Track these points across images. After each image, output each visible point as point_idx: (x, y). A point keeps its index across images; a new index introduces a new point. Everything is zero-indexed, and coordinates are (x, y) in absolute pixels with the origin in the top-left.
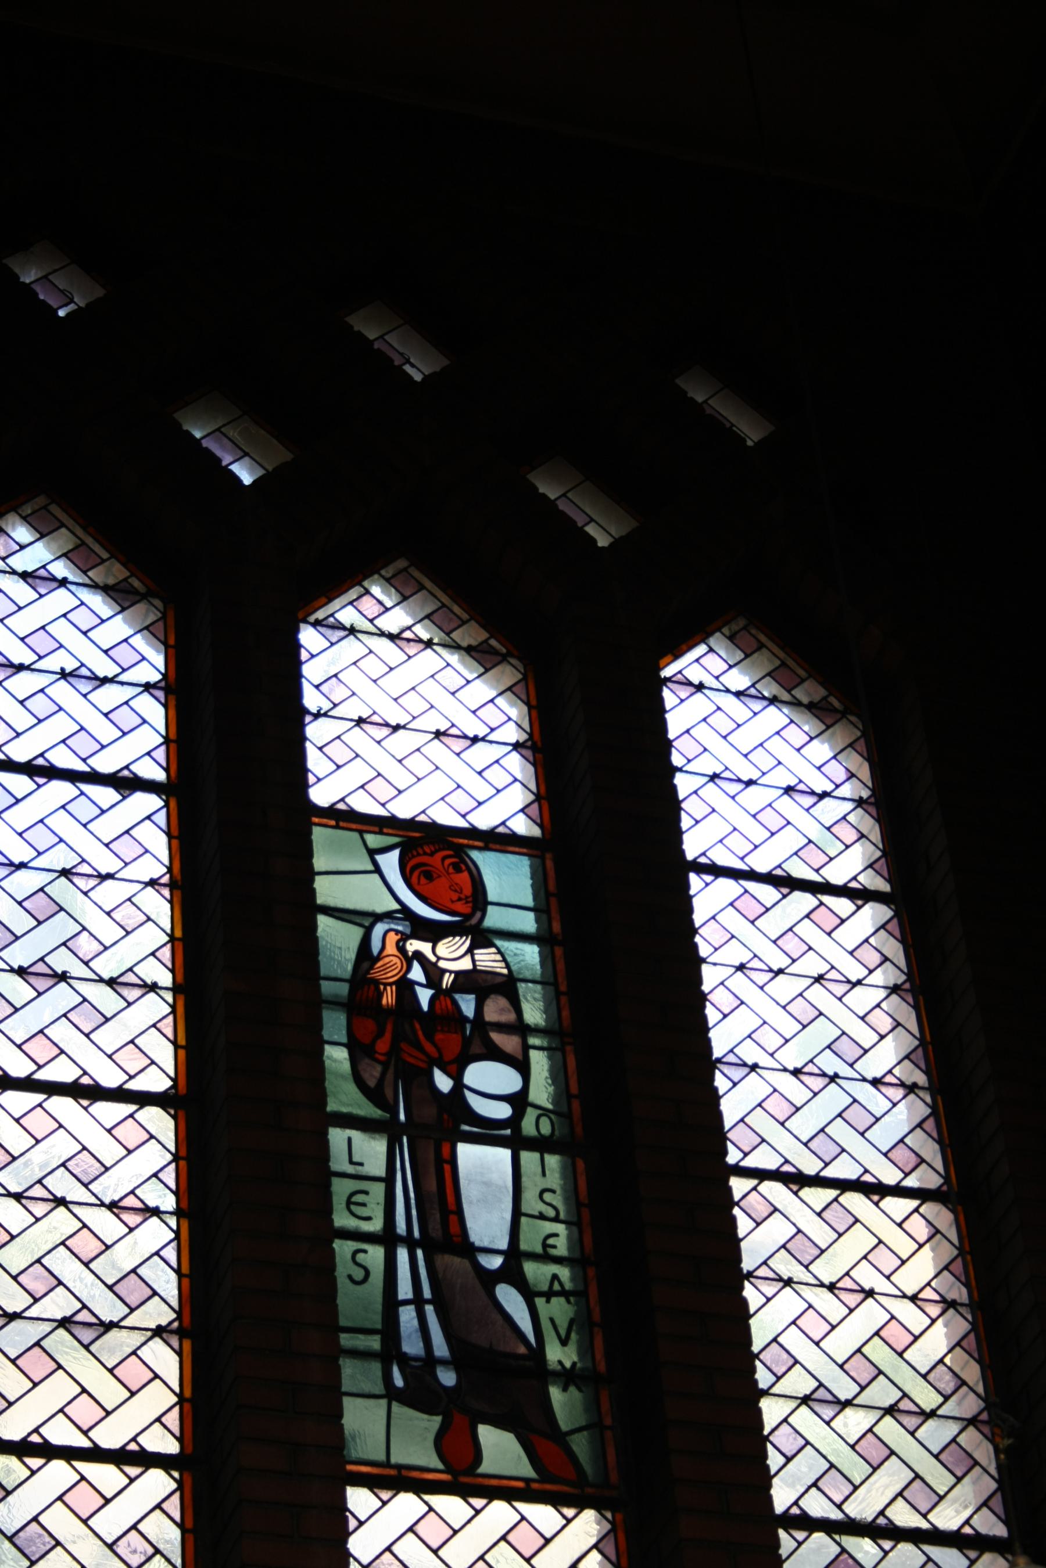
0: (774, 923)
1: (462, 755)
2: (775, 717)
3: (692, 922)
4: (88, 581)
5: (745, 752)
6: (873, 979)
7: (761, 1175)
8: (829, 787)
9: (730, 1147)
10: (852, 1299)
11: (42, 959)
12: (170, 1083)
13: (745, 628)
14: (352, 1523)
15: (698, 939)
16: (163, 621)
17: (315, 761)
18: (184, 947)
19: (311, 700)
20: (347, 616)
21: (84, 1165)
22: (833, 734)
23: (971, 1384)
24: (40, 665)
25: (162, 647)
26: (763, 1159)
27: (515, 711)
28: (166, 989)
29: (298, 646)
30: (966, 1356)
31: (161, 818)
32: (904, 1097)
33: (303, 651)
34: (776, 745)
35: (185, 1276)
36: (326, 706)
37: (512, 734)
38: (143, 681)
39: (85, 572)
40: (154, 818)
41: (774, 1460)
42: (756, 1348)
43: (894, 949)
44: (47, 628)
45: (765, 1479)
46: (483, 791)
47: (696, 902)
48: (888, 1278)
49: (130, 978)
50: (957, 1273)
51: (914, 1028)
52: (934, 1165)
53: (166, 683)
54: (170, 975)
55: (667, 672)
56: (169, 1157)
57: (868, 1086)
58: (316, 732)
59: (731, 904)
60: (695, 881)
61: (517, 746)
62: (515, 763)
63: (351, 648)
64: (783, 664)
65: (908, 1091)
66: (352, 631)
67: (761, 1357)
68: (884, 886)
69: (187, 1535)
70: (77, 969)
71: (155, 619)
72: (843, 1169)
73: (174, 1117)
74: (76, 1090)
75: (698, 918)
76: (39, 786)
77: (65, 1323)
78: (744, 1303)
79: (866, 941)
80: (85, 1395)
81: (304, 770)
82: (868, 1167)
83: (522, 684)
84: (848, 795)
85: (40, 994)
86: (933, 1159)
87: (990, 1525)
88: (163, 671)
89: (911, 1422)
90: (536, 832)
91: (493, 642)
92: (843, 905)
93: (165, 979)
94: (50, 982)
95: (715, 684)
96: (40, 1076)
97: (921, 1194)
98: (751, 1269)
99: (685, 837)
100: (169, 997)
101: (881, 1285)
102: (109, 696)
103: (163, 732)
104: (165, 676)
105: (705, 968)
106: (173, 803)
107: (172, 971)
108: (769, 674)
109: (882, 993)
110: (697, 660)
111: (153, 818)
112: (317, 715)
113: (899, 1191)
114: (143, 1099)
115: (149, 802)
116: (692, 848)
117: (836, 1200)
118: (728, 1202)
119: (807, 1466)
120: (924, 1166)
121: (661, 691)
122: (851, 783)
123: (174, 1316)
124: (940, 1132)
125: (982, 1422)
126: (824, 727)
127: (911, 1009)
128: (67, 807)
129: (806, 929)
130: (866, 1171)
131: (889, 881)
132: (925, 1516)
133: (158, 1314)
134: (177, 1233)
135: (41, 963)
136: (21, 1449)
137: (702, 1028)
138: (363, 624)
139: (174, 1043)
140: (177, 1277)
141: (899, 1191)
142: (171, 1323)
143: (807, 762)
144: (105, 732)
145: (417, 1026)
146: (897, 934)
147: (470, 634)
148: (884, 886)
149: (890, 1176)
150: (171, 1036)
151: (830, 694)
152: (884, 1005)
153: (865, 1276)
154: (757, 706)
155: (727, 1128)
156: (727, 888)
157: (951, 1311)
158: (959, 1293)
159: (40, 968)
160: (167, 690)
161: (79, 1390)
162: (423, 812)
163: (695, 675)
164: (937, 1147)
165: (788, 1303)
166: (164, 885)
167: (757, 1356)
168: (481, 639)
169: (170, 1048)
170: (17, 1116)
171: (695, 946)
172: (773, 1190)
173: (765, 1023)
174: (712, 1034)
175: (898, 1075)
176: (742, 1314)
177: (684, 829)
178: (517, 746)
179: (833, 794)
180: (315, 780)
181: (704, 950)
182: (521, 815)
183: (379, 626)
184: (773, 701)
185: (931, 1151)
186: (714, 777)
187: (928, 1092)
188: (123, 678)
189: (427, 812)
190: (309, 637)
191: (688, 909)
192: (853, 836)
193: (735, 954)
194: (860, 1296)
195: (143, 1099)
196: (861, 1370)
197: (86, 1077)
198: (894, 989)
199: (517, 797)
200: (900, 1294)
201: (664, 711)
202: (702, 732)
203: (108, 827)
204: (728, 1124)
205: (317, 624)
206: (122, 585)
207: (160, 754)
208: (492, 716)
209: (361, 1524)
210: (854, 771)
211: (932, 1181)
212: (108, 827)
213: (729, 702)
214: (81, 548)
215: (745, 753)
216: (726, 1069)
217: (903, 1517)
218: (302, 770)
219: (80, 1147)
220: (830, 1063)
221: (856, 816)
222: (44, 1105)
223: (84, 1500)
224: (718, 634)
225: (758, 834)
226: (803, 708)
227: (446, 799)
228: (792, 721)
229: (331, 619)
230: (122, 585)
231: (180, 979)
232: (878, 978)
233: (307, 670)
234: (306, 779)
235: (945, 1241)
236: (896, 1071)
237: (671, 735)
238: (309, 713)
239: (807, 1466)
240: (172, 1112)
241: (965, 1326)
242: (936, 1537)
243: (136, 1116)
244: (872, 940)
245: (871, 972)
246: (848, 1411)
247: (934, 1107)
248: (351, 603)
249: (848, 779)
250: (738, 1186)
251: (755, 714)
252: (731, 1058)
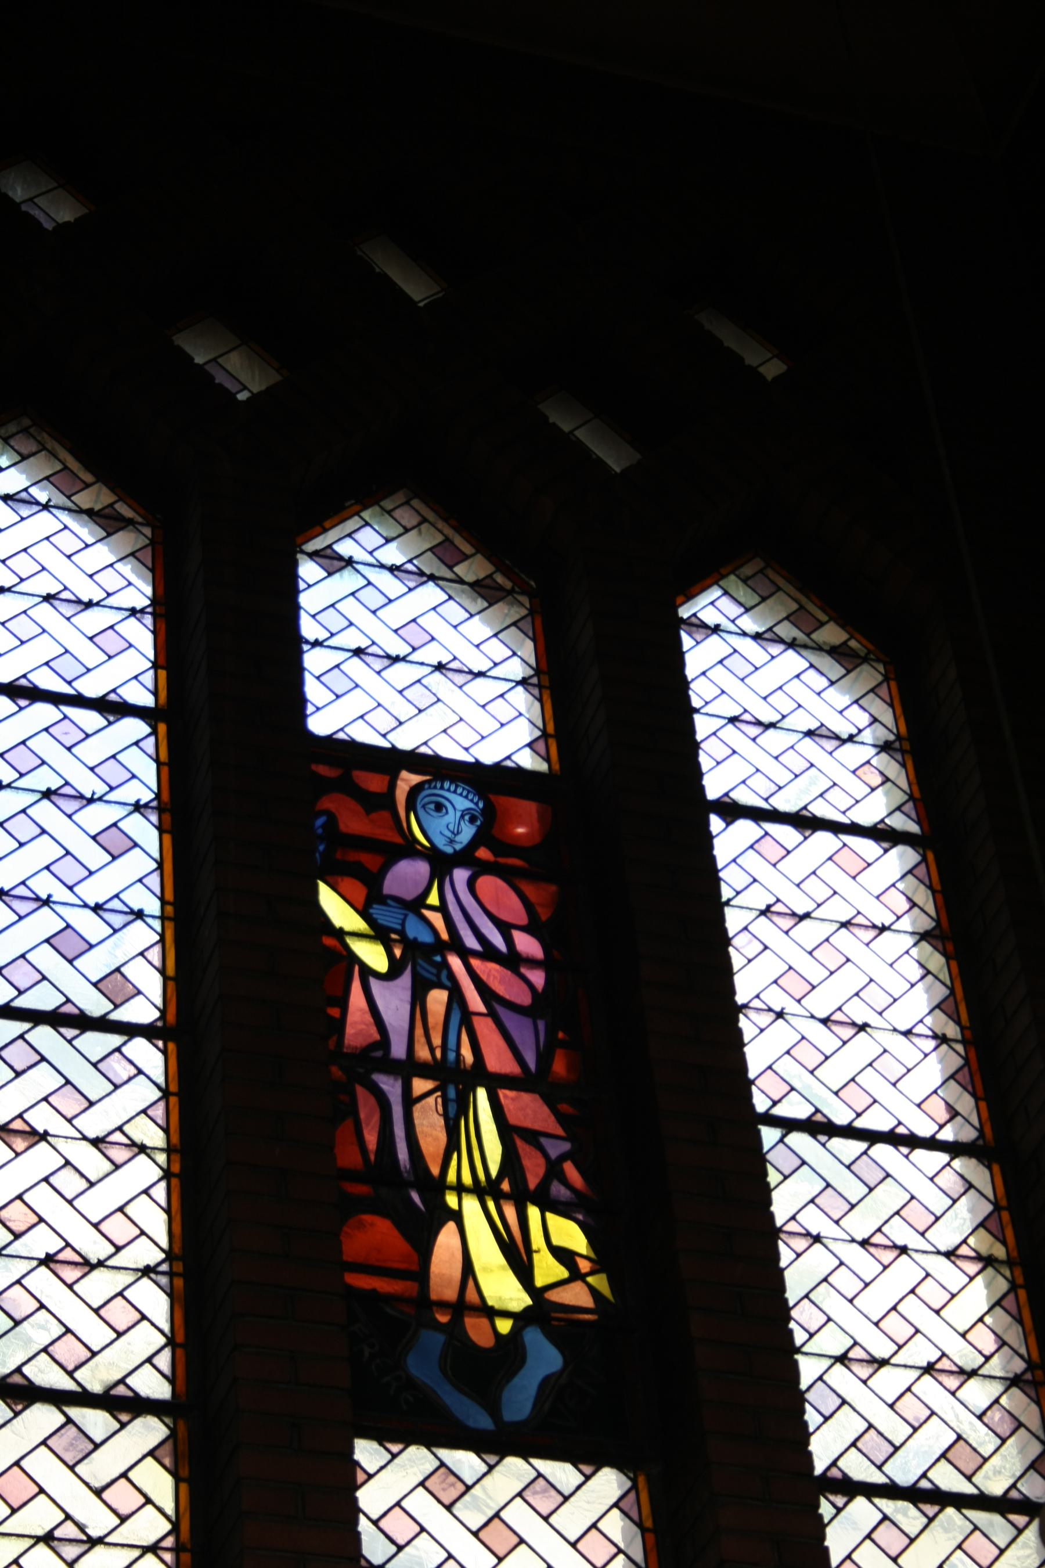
0: (797, 865)
1: (464, 688)
2: (793, 661)
3: (725, 931)
4: (69, 504)
5: (775, 755)
6: (900, 925)
7: (789, 1125)
8: (809, 906)
9: (770, 1169)
10: (887, 1256)
11: (23, 883)
12: (157, 1014)
13: (761, 571)
14: (361, 1477)
15: (691, 693)
16: (164, 1100)
17: (313, 690)
18: (170, 770)
19: (309, 629)
20: (346, 548)
21: (69, 871)
22: (855, 680)
23: (921, 904)
24: (22, 587)
25: (150, 575)
26: (794, 1109)
27: (528, 650)
28: (153, 917)
29: (294, 577)
30: (959, 1089)
31: (149, 744)
32: (935, 1049)
33: (309, 705)
34: (795, 688)
35: (164, 764)
36: (322, 635)
37: (516, 669)
38: (129, 605)
39: (69, 497)
40: (141, 744)
41: (812, 1418)
42: (752, 1075)
43: (924, 896)
44: (28, 956)
45: (804, 1435)
46: (487, 724)
47: (688, 658)
48: (923, 1234)
49: (116, 904)
50: (921, 876)
51: (903, 783)
52: (971, 1121)
53: (159, 803)
54: (161, 1134)
55: (685, 612)
56: (162, 1340)
57: (943, 1260)
58: (314, 661)
59: (775, 982)
60: (716, 823)
61: (523, 682)
62: (520, 698)
63: (346, 581)
64: (801, 607)
65: (939, 1041)
66: (716, 629)
67: (757, 1082)
68: (914, 828)
69: (173, 1157)
70: (61, 894)
71: (144, 544)
72: (876, 1121)
73: (164, 1052)
74: (55, 1019)
75: (690, 672)
76: (21, 709)
77: (48, 1261)
78: (740, 1033)
79: (893, 885)
80: (69, 1197)
81: (303, 701)
82: (921, 1238)
83: (529, 619)
84: (999, 1373)
85: (21, 918)
86: (925, 904)
87: (900, 822)
88: (156, 790)
89: (864, 1371)
90: (543, 767)
91: (853, 644)
92: (868, 848)
93: (153, 906)
94: (34, 905)
95: (732, 627)
96: (22, 1026)
97: (954, 1149)
98: (745, 1001)
99: (716, 841)
100: (157, 925)
101: (913, 1241)
102: (94, 620)
103: (152, 658)
104: (158, 796)
105: (697, 717)
106: (930, 856)
107: (166, 1130)
108: (787, 618)
109: (910, 941)
110: (712, 603)
111: (141, 744)
112: (317, 643)
113: (931, 1144)
114: (130, 1030)
115: (135, 728)
116: (714, 788)
117: (865, 1153)
118: (759, 1161)
119: (847, 1425)
120: (1022, 1430)
121: (737, 1020)
122: (991, 1317)
123: (153, 796)
124: (973, 1087)
125: (1027, 1382)
126: (844, 671)
127: (886, 706)
128: (51, 664)
129: (829, 872)
130: (907, 1157)
131: (919, 822)
132: (969, 1478)
133: (148, 1254)
134: (162, 936)
135: (22, 913)
136: (13, 690)
137: (726, 972)
138: (359, 555)
139: (157, 761)
140: (153, 636)
141: (931, 1144)
142: (159, 1264)
143: (866, 887)
144: (91, 655)
145: (410, 838)
146: (913, 815)
147: (831, 634)
148: (914, 828)
149: (924, 1129)
150: (158, 891)
151: (852, 637)
152: (988, 1320)
153: (898, 1231)
154: (775, 649)
155: (765, 1149)
156: (745, 829)
157: (944, 1047)
158: (952, 1030)
159: (22, 891)
160: (160, 810)
161: (63, 1081)
162: (425, 743)
163: (710, 617)
164: (929, 892)
165: (781, 1035)
166: (163, 1273)
167: (752, 1082)
168: (489, 572)
169: (153, 766)
170: (95, 1220)
171: (688, 698)
172: (799, 1140)
173: (803, 1038)
174: (746, 1049)
175: (972, 1245)
176: (736, 1042)
177: (714, 833)
178: (523, 682)
179: (409, 658)
180: (314, 709)
181: (696, 702)
182: (527, 750)
183: (380, 559)
184: (792, 645)
185: (966, 1104)
186: (733, 720)
187: (512, 1202)
188: (332, 642)
189: (429, 743)
190: (308, 570)
191: (780, 1286)
192: (877, 780)
193: (758, 898)
194: (894, 1253)
195: (130, 1030)
196: (909, 1407)
197: (69, 1005)
198: (923, 937)
199: (523, 732)
200: (766, 1008)
201: (700, 775)
202: (719, 674)
203: (93, 751)
204: (720, 864)
205: (313, 555)
206: (107, 511)
207: (148, 679)
208: (110, 580)
209: (370, 1476)
210: (876, 715)
211: (968, 1135)
212: (93, 751)
213: (748, 646)
214: (64, 472)
215: (775, 755)
216: (752, 1014)
217: (948, 1479)
218: (302, 701)
219: (63, 1244)
220: (858, 1013)
221: (1009, 1398)
222: (26, 1036)
223: (69, 1351)
224: (732, 577)
225: (782, 776)
226: (824, 654)
227: (438, 609)
228: (812, 666)
229: (329, 551)
230: (107, 511)
231: (175, 1139)
232: (905, 924)
233: (304, 599)
234: (296, 585)
235: (895, 788)
236: (971, 1241)
237: (699, 737)
238: (307, 642)
239: (847, 1425)
240: (160, 1044)
241: (958, 1062)
242: (982, 1502)
243: (124, 1049)
244: (939, 1092)
245: (898, 918)
246: (885, 1370)
247: (966, 1059)
248: (349, 535)
249: (883, 784)
250: (769, 1135)
251: (773, 657)
252: (756, 1003)
